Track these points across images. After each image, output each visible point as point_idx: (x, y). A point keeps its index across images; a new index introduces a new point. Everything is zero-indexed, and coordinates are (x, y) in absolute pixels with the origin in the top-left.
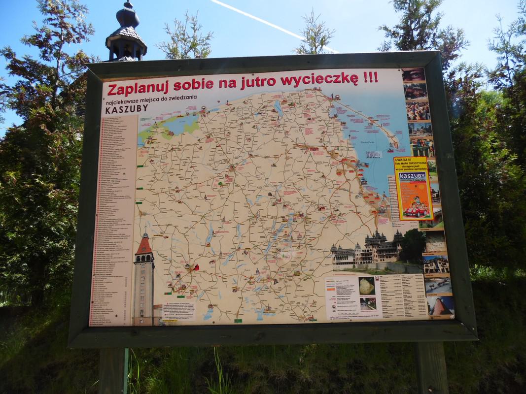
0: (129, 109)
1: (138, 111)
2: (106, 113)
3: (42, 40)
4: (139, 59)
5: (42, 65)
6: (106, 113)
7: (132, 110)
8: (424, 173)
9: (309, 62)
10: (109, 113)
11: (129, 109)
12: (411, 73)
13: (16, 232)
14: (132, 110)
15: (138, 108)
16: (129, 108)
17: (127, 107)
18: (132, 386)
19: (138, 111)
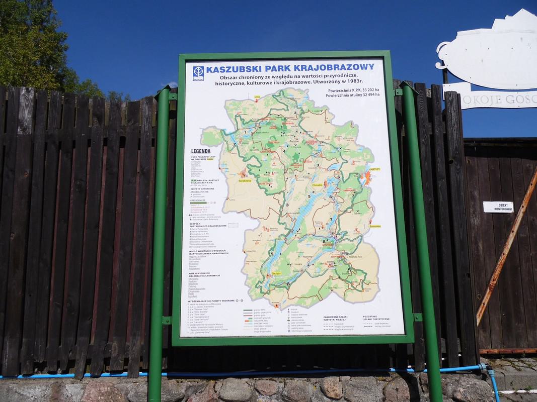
1: (240, 71)
2: (295, 70)
6: (295, 70)
7: (235, 70)
11: (231, 70)
14: (235, 70)
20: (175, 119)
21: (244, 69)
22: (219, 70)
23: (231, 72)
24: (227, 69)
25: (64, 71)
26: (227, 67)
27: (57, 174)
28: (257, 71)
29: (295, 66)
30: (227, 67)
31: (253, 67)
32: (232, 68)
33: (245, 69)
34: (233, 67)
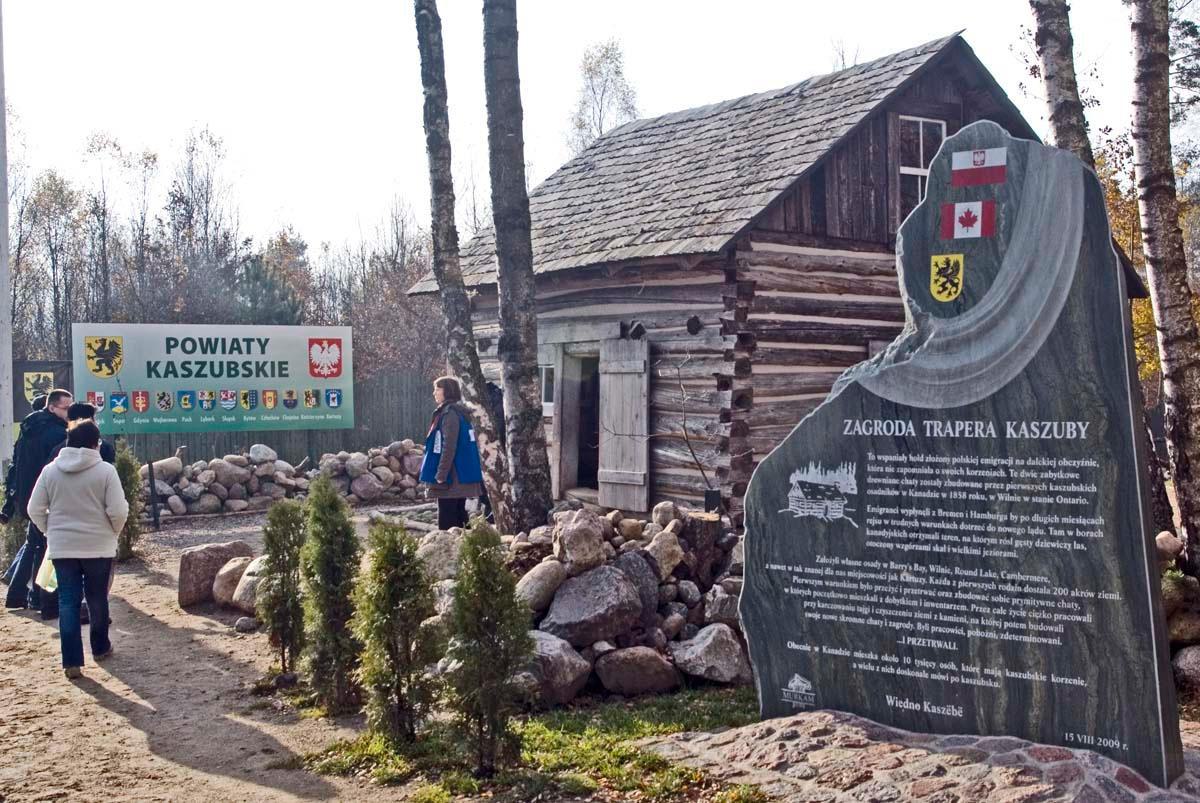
0: (206, 370)
1: (229, 375)
2: (149, 376)
3: (812, 467)
4: (880, 657)
5: (1184, 675)
6: (149, 376)
7: (217, 371)
8: (338, 342)
9: (617, 73)
10: (158, 376)
11: (206, 370)
12: (806, 604)
13: (1096, 595)
14: (217, 371)
15: (229, 369)
16: (208, 366)
17: (203, 364)
18: (234, 462)
19: (229, 375)
20: (1003, 728)
21: (235, 369)
22: (180, 371)
23: (205, 376)
24: (203, 372)
25: (518, 520)
26: (197, 363)
27: (661, 287)
28: (266, 375)
29: (149, 363)
30: (197, 363)
31: (257, 363)
32: (208, 366)
33: (240, 368)
34: (212, 363)
